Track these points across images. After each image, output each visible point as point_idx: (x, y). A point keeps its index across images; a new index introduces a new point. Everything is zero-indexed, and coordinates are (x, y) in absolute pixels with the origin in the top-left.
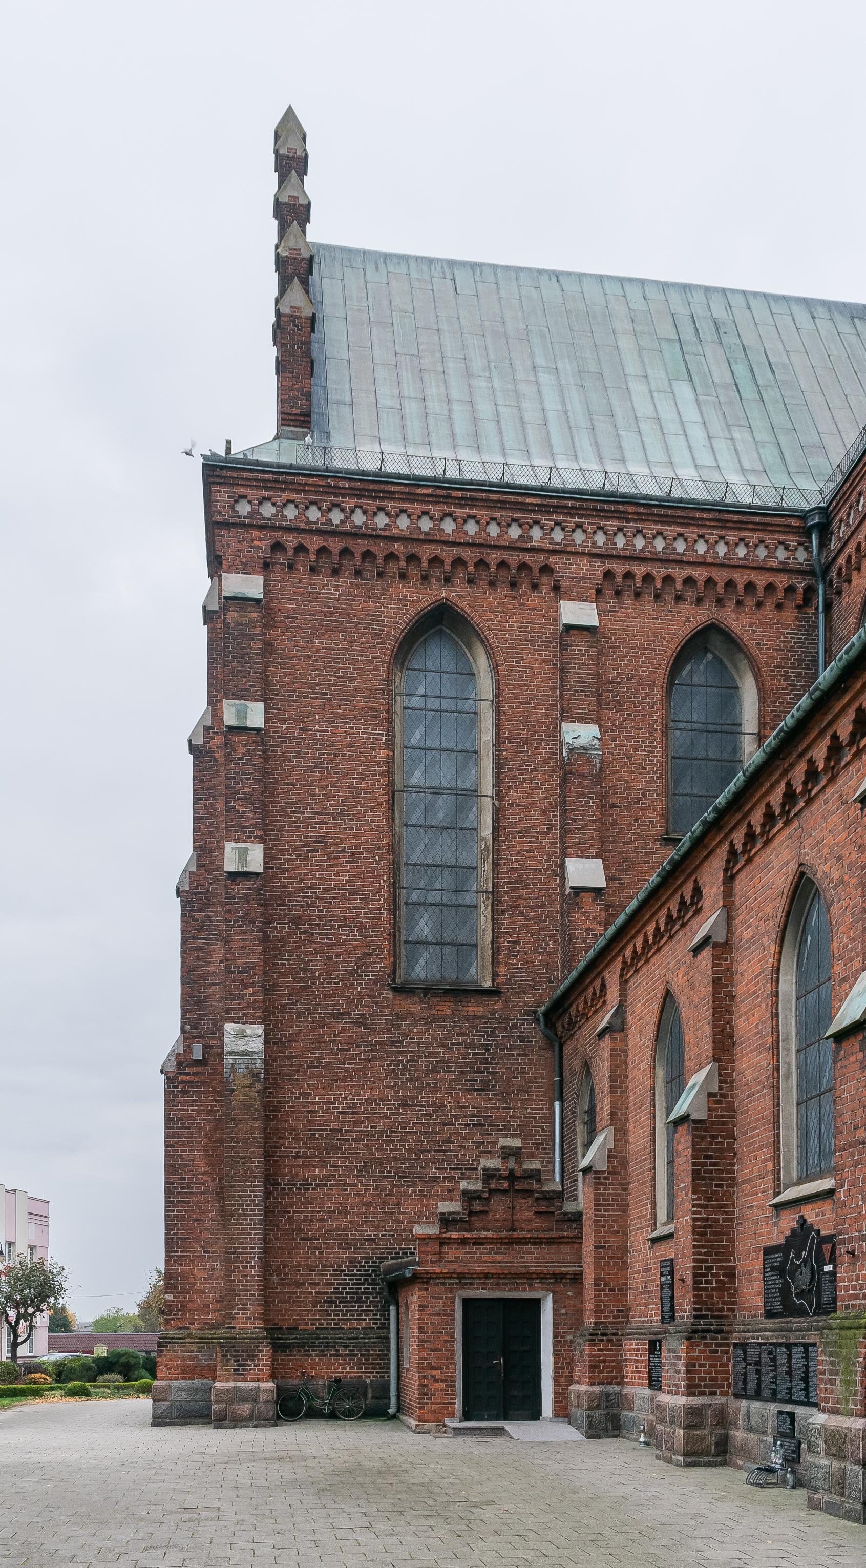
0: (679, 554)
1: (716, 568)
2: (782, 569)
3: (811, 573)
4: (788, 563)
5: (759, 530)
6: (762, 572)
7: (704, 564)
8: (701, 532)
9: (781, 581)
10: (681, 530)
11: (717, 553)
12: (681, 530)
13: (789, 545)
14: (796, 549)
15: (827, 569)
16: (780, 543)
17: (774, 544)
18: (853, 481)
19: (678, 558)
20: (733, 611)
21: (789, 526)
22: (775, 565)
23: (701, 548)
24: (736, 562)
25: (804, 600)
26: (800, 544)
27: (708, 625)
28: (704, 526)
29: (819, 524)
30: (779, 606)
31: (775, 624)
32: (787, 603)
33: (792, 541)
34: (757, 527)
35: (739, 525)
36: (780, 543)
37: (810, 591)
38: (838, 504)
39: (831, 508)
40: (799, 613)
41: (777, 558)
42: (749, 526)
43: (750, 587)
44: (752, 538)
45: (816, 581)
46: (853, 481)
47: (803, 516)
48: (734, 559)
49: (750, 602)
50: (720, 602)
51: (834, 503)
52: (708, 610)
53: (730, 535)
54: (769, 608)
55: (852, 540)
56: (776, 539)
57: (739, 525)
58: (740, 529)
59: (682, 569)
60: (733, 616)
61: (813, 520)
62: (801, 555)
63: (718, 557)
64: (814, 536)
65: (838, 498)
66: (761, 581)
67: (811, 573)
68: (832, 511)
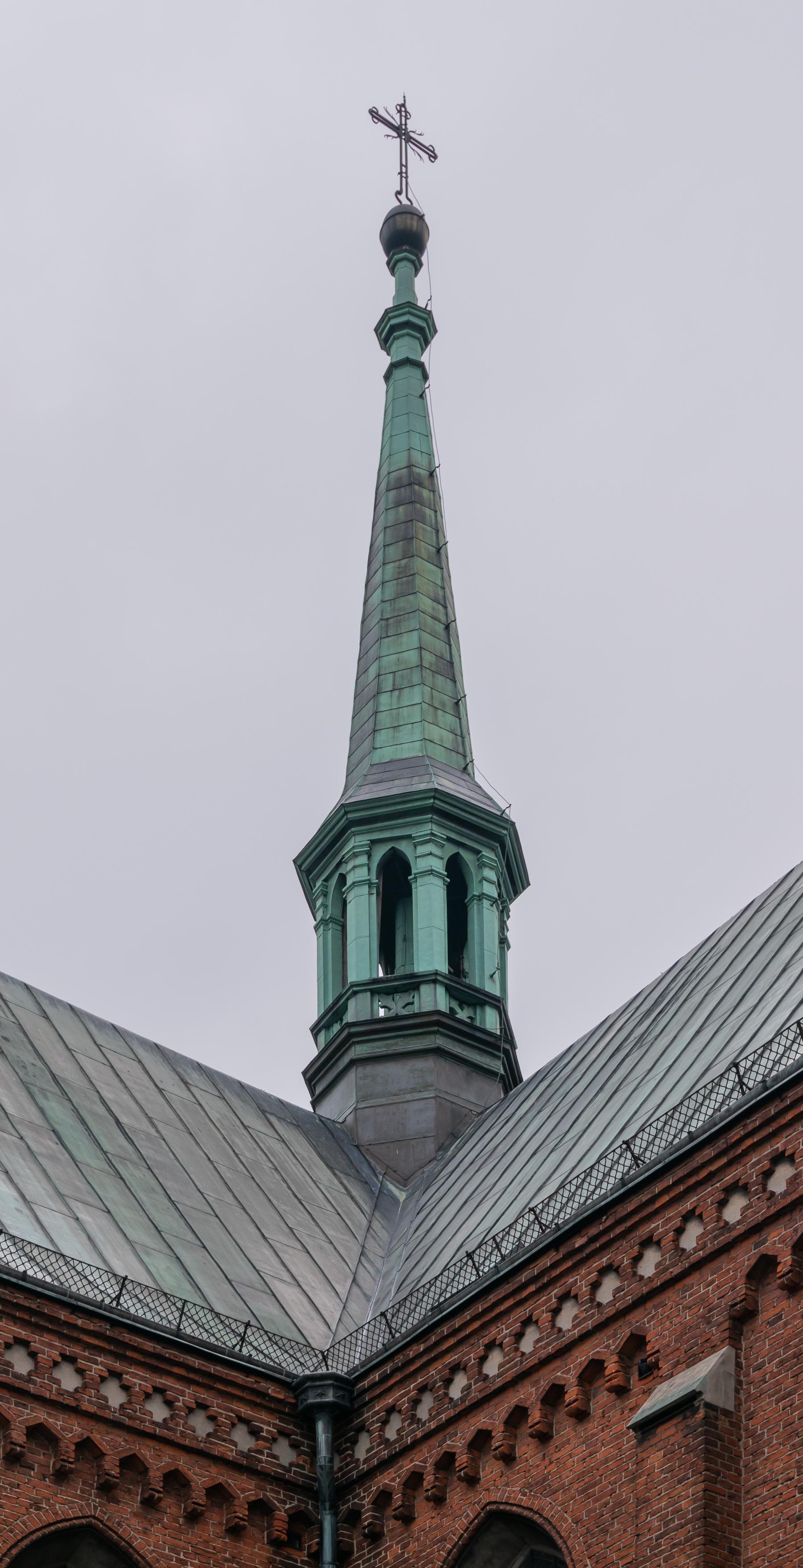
0: (17, 1376)
1: (102, 1427)
2: (244, 1466)
3: (308, 1490)
4: (260, 1461)
5: (198, 1384)
6: (203, 1462)
7: (75, 1411)
8: (69, 1350)
9: (245, 1489)
10: (23, 1333)
11: (106, 1399)
12: (23, 1333)
13: (262, 1430)
14: (274, 1440)
15: (343, 1489)
16: (242, 1420)
17: (228, 1417)
18: (437, 1344)
19: (17, 1383)
20: (135, 1515)
21: (263, 1395)
22: (231, 1455)
23: (69, 1380)
24: (147, 1427)
25: (289, 1533)
26: (282, 1433)
27: (81, 1526)
28: (78, 1341)
29: (345, 1402)
30: (508, 1459)
31: (226, 1560)
32: (252, 1531)
33: (269, 1424)
34: (192, 1376)
35: (154, 1362)
36: (242, 1420)
37: (302, 1523)
38: (384, 1378)
39: (366, 1383)
40: (275, 1553)
41: (235, 1444)
42: (176, 1370)
43: (175, 1480)
44: (183, 1394)
45: (316, 1507)
46: (437, 1344)
47: (298, 1386)
48: (143, 1421)
49: (172, 1508)
50: (107, 1489)
51: (376, 1376)
52: (81, 1498)
53: (134, 1375)
54: (526, 1449)
55: (434, 1441)
56: (232, 1411)
57: (154, 1362)
58: (155, 1370)
59: (25, 1406)
60: (135, 1522)
61: (322, 1395)
62: (285, 1454)
63: (109, 1408)
64: (320, 1426)
65: (388, 1368)
66: (201, 1476)
67: (308, 1490)
68: (365, 1391)
